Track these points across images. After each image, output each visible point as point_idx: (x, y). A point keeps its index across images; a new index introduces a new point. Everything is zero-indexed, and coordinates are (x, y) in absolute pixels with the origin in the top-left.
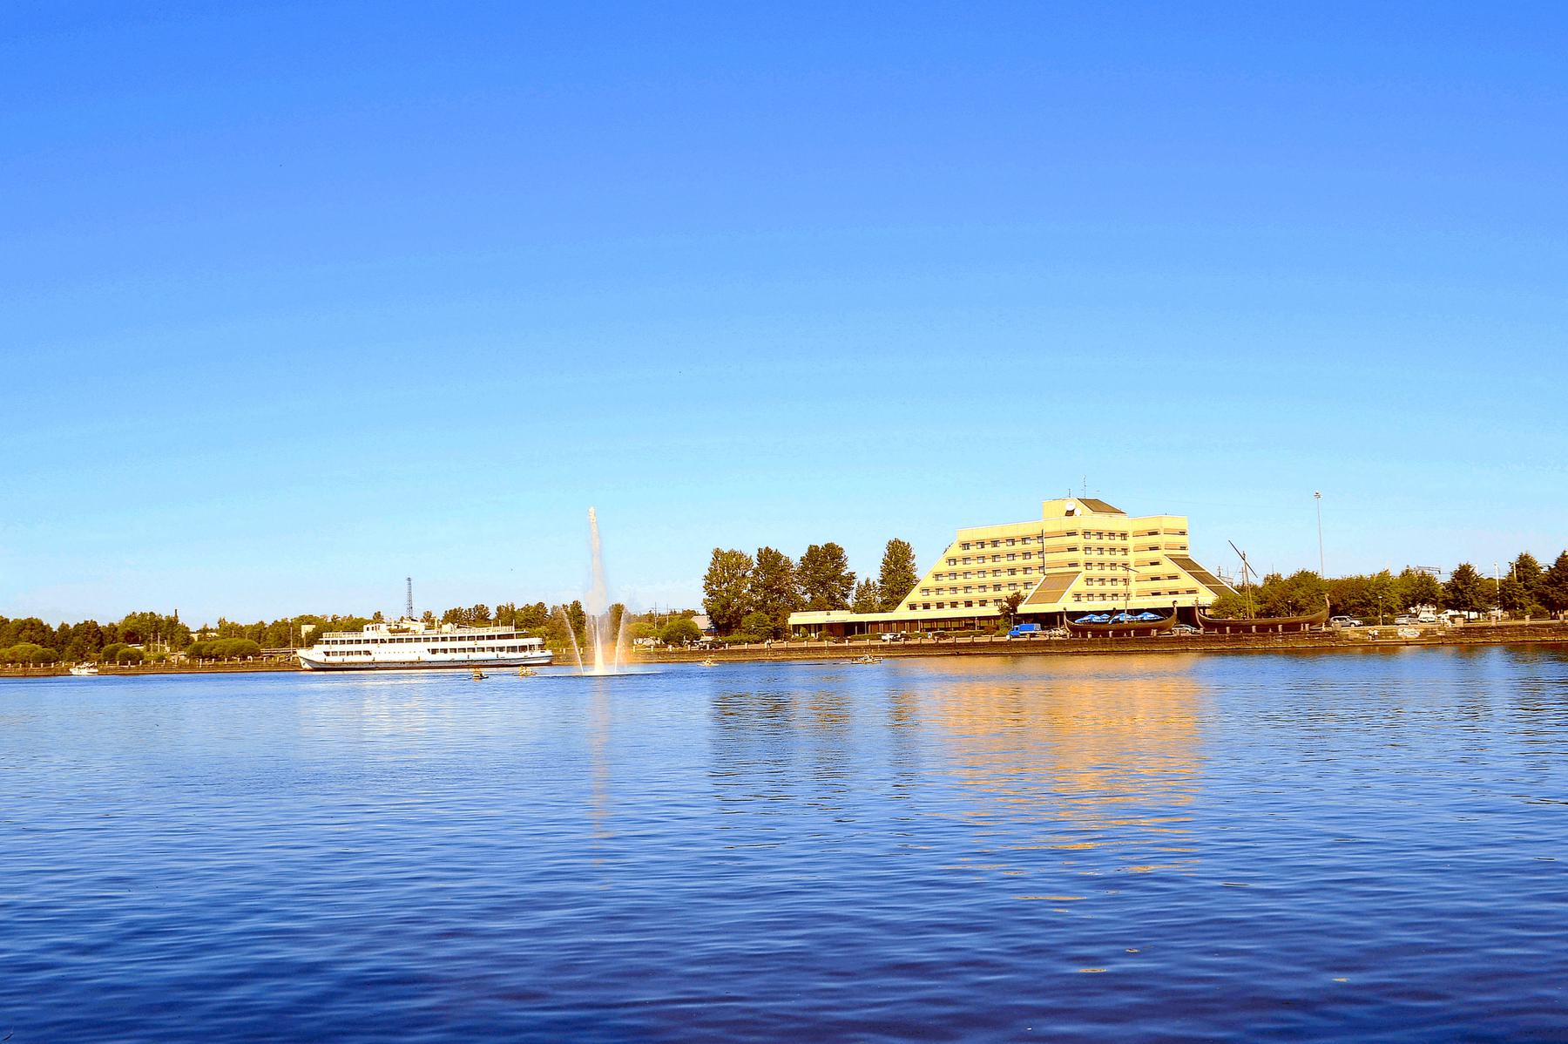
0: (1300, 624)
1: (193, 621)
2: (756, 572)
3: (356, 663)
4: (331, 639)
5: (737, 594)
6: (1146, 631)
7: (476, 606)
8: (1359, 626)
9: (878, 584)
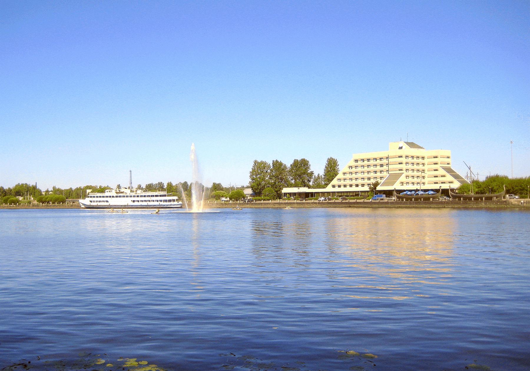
0: (492, 197)
1: (43, 187)
2: (271, 170)
3: (103, 206)
4: (92, 196)
5: (263, 179)
6: (428, 199)
7: (159, 183)
8: (518, 198)
9: (323, 176)
